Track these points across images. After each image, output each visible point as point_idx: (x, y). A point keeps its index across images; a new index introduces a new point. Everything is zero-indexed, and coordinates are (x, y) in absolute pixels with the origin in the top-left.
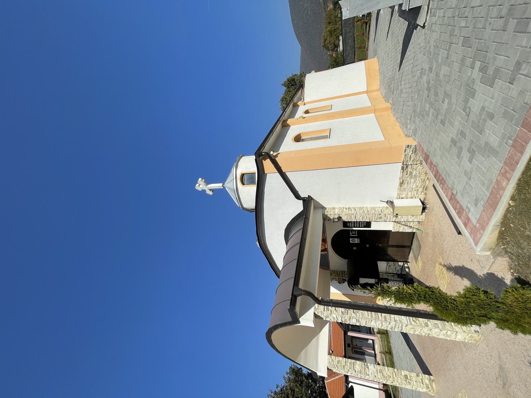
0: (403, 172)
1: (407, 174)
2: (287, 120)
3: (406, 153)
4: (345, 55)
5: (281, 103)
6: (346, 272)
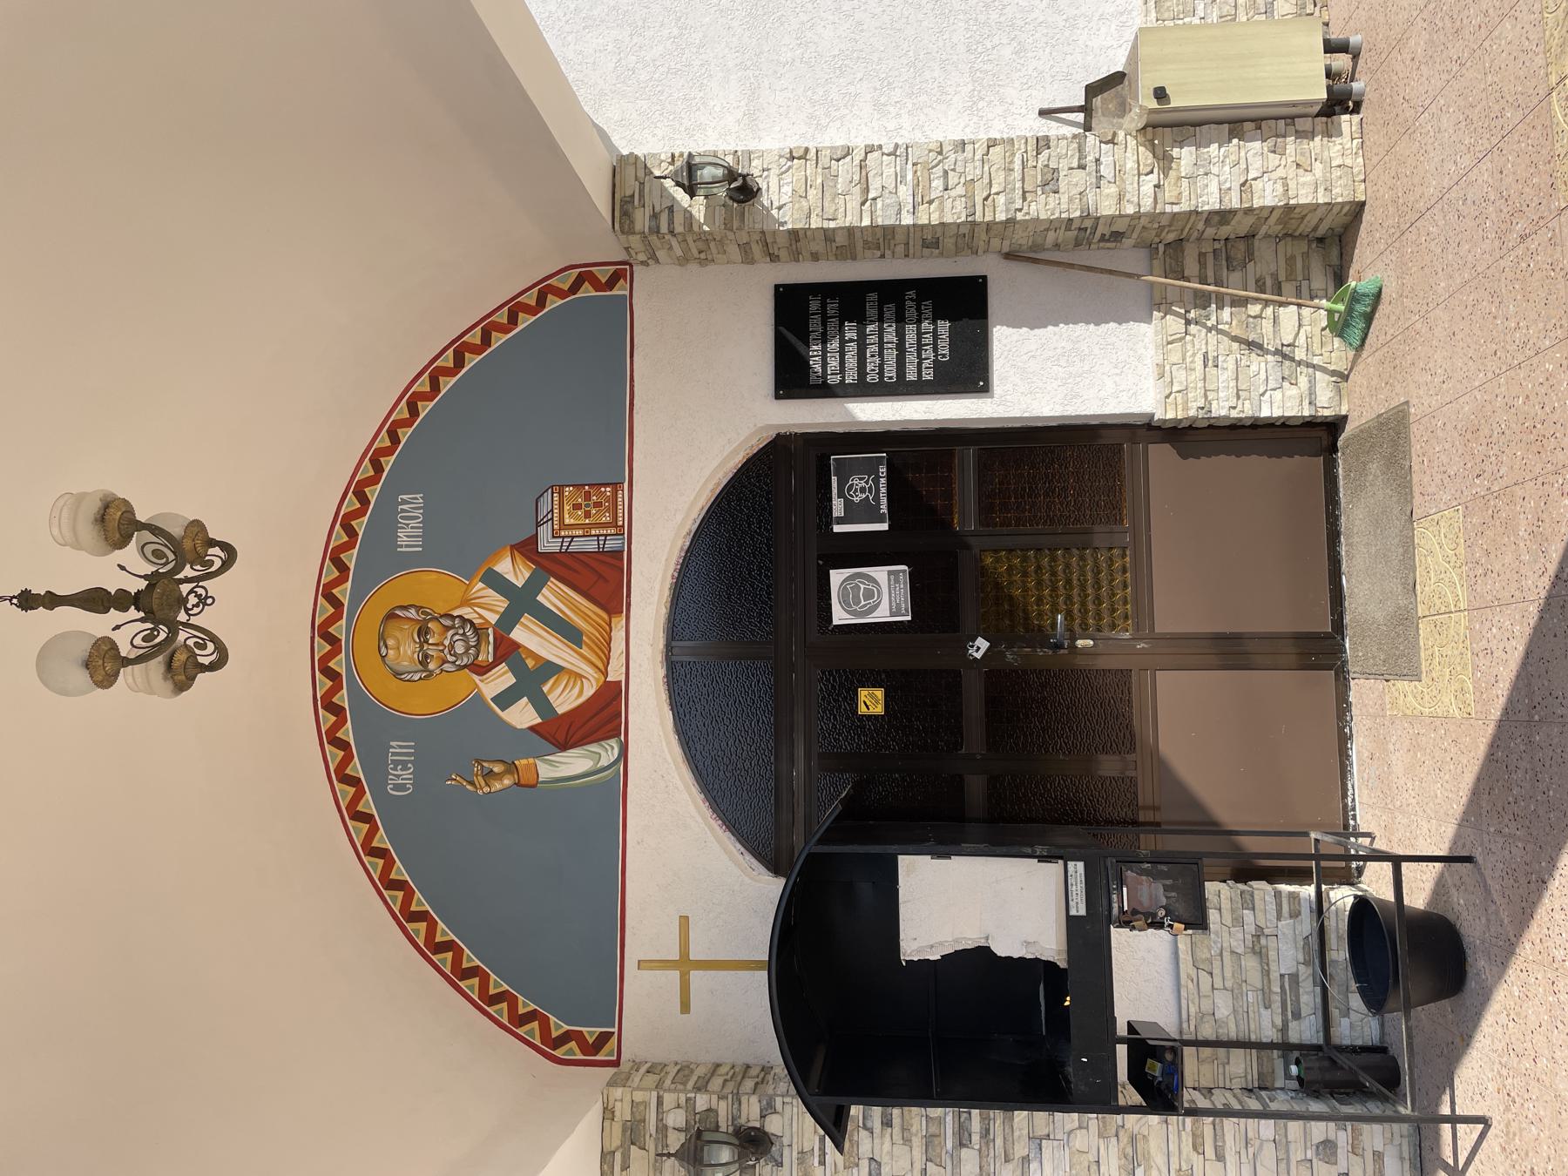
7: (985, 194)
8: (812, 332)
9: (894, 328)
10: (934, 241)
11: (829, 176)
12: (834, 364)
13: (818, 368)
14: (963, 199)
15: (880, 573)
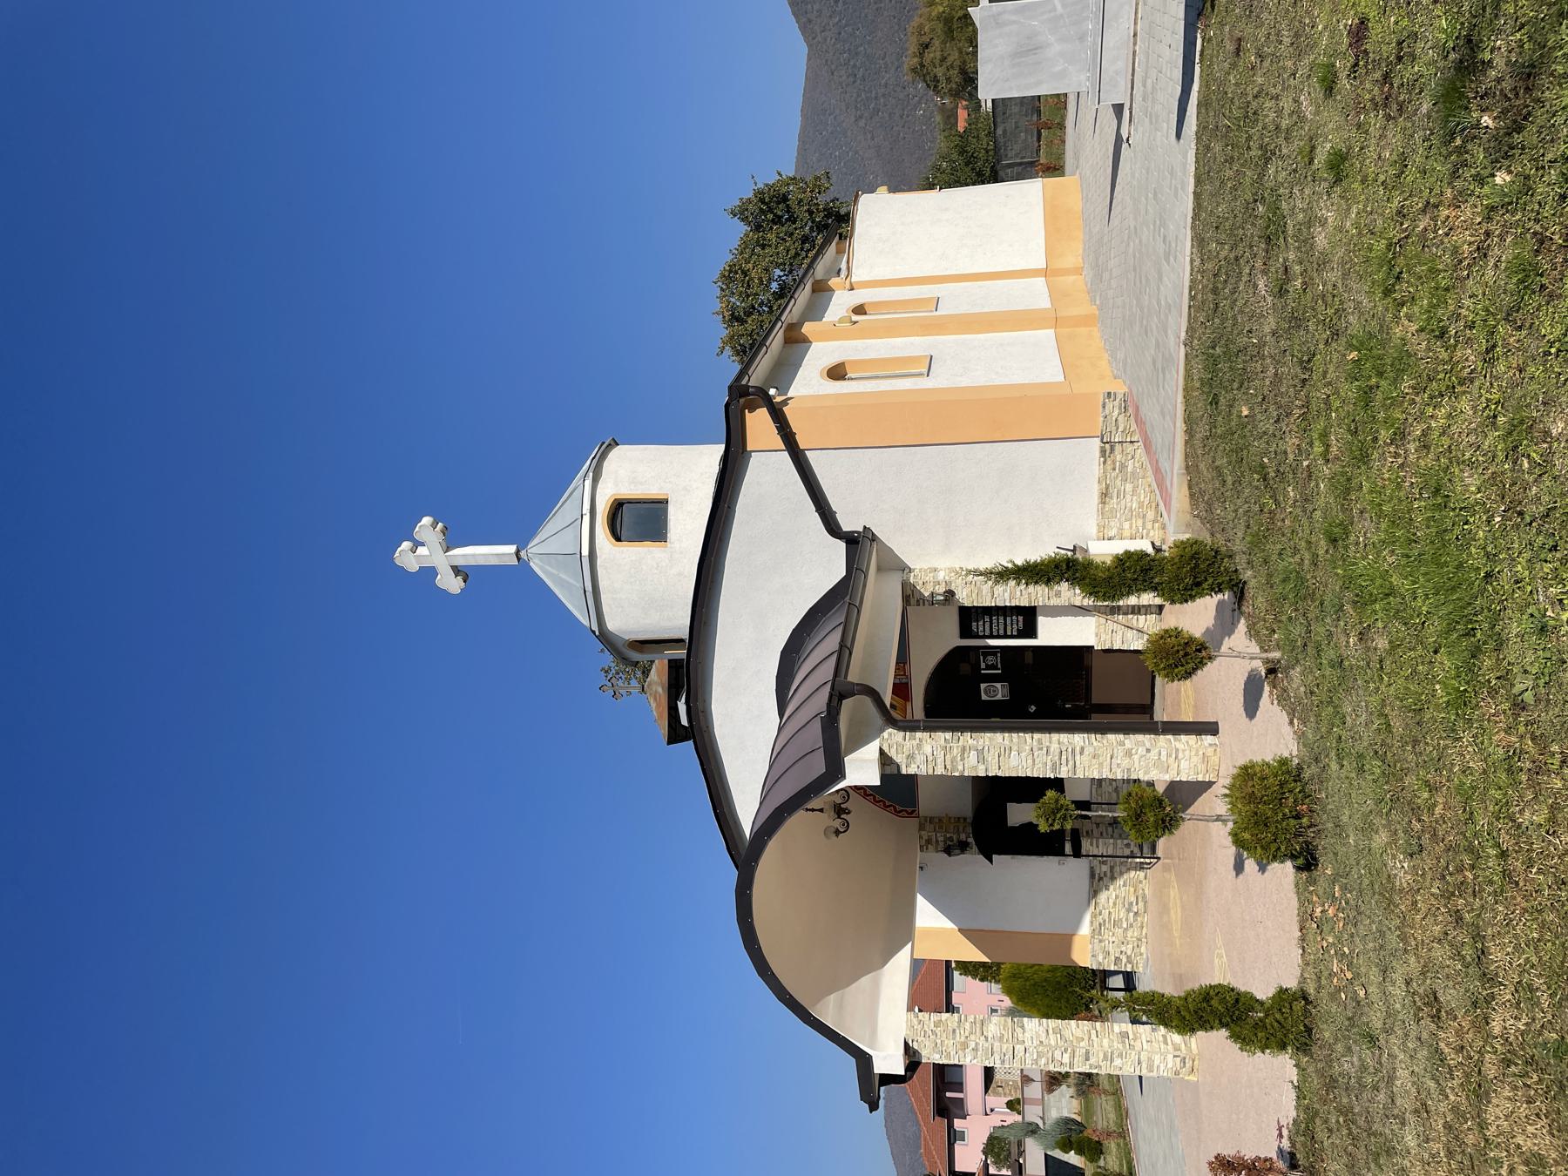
0: (1105, 463)
1: (1114, 469)
2: (800, 324)
3: (1107, 412)
4: (999, 132)
5: (722, 289)
6: (969, 821)
15: (998, 685)
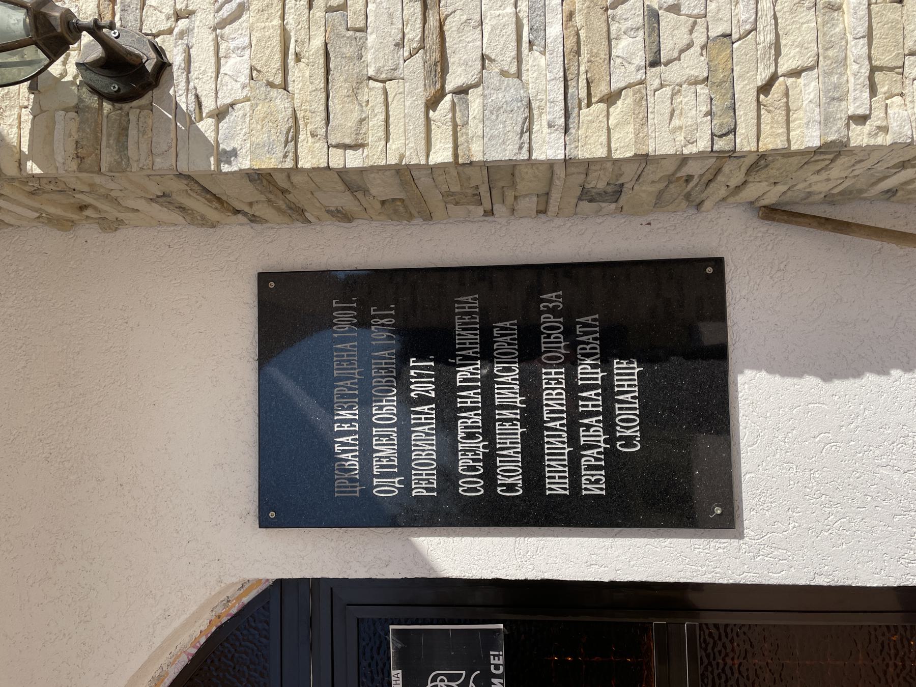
7: (762, 77)
8: (340, 379)
9: (515, 374)
10: (610, 189)
11: (342, 29)
12: (387, 451)
13: (352, 460)
14: (702, 90)
